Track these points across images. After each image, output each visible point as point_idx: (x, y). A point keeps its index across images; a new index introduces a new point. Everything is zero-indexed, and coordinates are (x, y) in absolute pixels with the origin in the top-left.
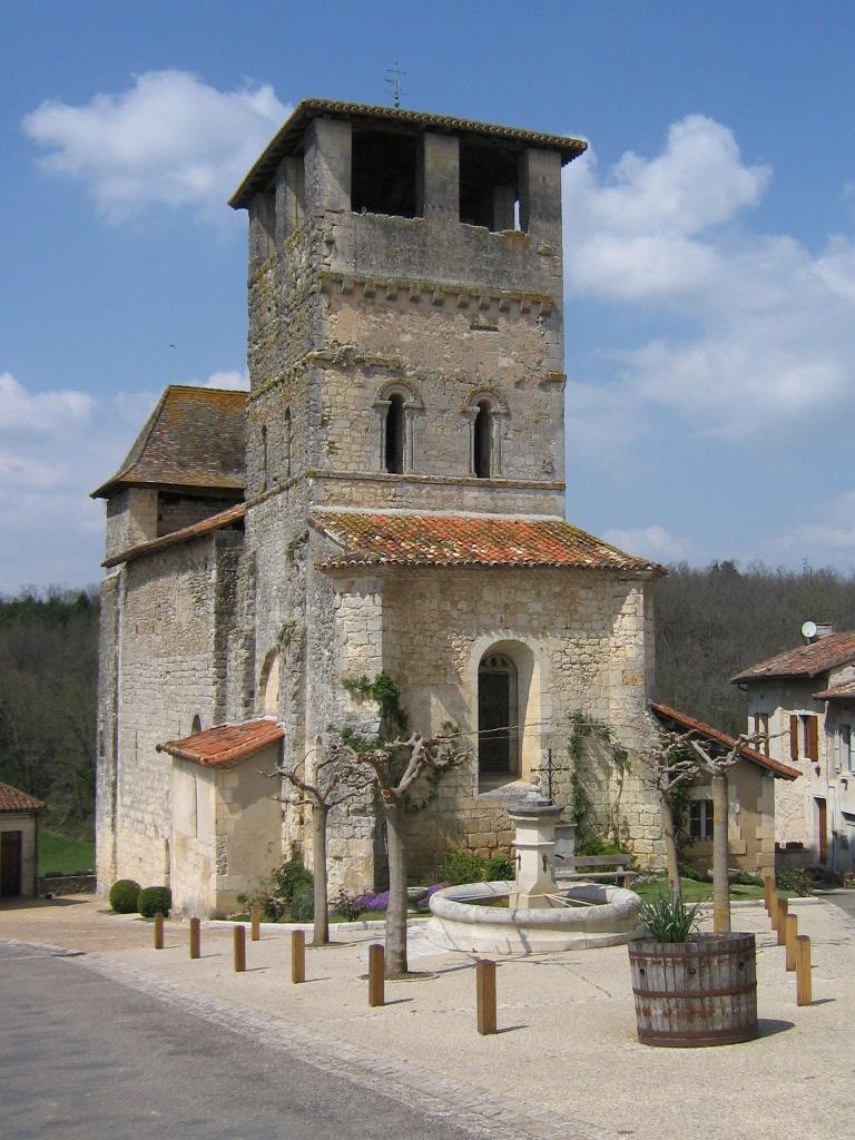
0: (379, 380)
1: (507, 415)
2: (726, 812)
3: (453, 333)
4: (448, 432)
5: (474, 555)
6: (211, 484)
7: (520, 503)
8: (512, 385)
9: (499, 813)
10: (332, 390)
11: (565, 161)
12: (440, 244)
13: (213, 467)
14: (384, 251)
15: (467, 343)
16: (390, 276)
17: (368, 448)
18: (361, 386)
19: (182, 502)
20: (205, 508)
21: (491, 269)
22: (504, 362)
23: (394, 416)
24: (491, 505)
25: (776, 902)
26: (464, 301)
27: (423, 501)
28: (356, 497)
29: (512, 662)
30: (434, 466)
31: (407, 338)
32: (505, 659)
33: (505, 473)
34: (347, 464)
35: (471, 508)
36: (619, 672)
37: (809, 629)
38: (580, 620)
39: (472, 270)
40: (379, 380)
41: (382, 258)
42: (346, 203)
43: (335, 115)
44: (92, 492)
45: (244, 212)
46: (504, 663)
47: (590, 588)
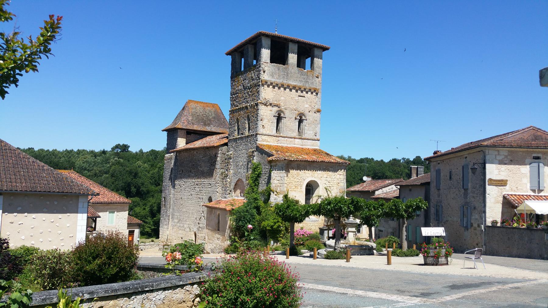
0: (275, 109)
1: (306, 120)
2: (493, 183)
3: (294, 97)
4: (292, 124)
5: (272, 152)
6: (202, 130)
7: (309, 144)
8: (308, 112)
9: (309, 225)
10: (264, 111)
11: (323, 51)
12: (291, 73)
13: (201, 125)
14: (278, 74)
15: (297, 100)
16: (279, 81)
17: (272, 127)
18: (271, 111)
19: (192, 134)
20: (198, 136)
21: (304, 81)
22: (307, 106)
23: (279, 119)
24: (301, 144)
25: (539, 156)
26: (297, 89)
27: (285, 142)
28: (269, 140)
29: (311, 185)
30: (288, 133)
31: (282, 98)
32: (310, 185)
33: (305, 135)
34: (267, 131)
35: (298, 144)
36: (339, 189)
37: (365, 178)
38: (330, 176)
39: (299, 81)
40: (275, 109)
41: (277, 76)
42: (269, 61)
43: (267, 36)
44: (163, 129)
45: (230, 57)
46: (310, 186)
47: (332, 167)
